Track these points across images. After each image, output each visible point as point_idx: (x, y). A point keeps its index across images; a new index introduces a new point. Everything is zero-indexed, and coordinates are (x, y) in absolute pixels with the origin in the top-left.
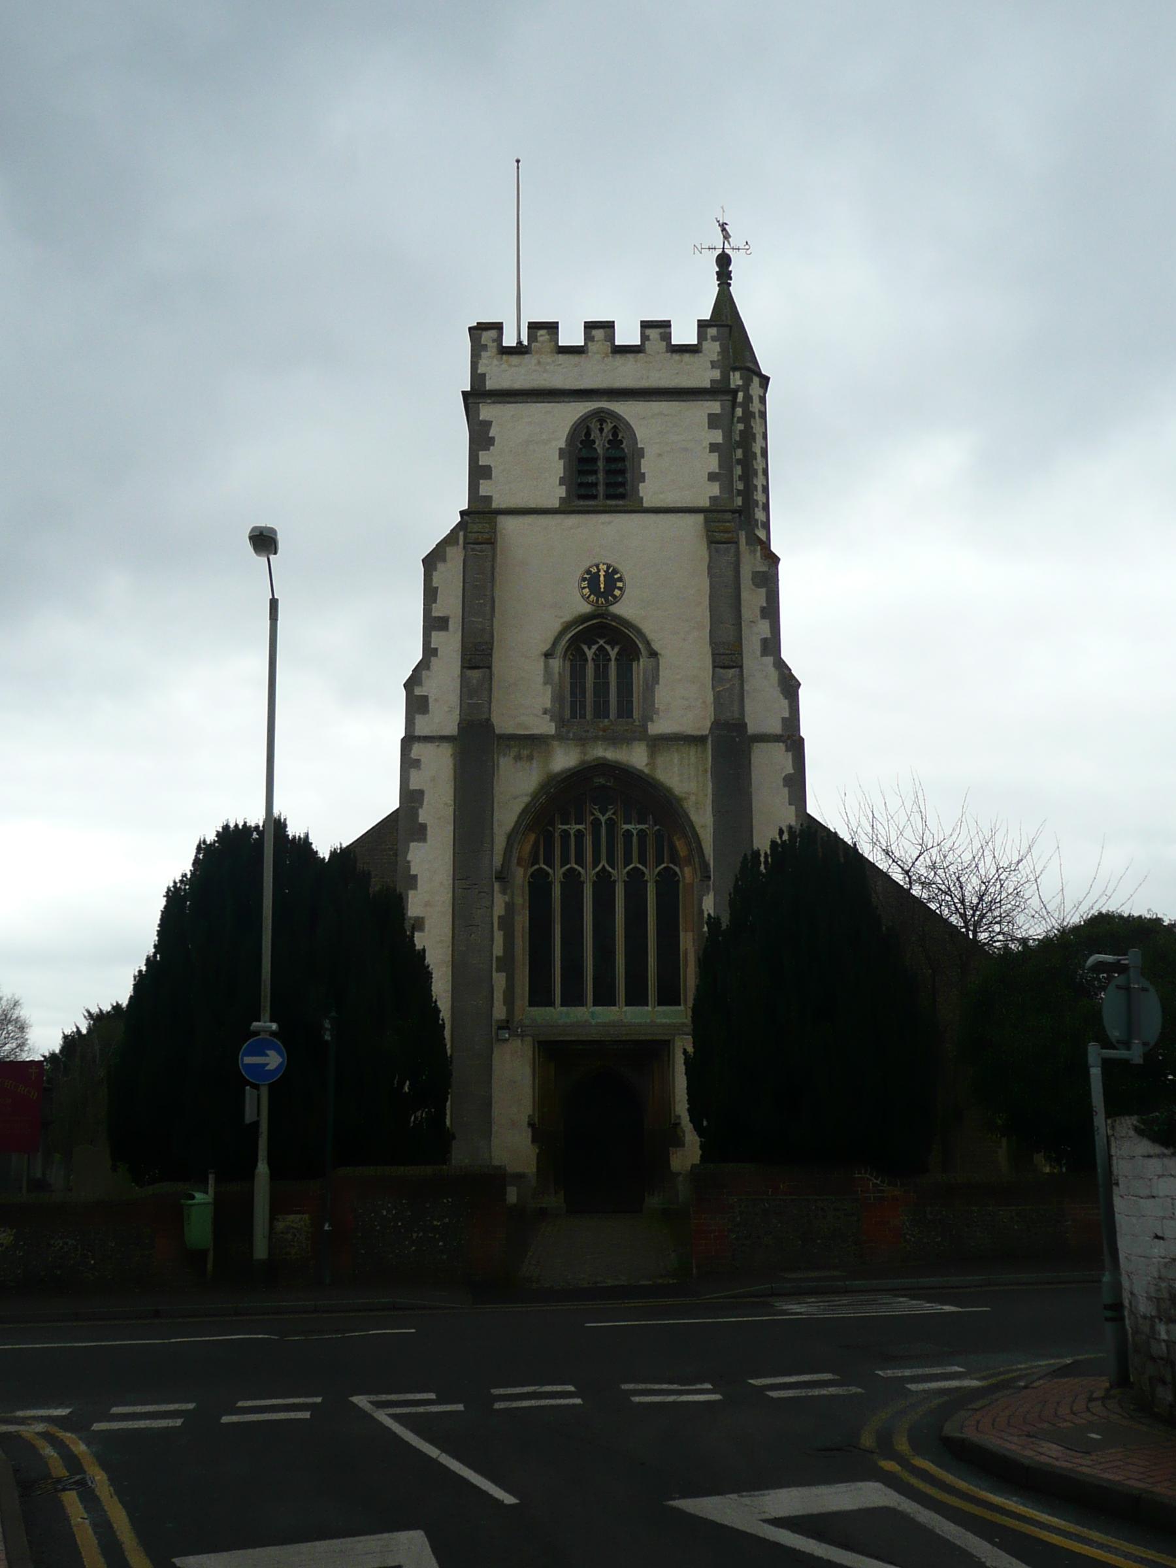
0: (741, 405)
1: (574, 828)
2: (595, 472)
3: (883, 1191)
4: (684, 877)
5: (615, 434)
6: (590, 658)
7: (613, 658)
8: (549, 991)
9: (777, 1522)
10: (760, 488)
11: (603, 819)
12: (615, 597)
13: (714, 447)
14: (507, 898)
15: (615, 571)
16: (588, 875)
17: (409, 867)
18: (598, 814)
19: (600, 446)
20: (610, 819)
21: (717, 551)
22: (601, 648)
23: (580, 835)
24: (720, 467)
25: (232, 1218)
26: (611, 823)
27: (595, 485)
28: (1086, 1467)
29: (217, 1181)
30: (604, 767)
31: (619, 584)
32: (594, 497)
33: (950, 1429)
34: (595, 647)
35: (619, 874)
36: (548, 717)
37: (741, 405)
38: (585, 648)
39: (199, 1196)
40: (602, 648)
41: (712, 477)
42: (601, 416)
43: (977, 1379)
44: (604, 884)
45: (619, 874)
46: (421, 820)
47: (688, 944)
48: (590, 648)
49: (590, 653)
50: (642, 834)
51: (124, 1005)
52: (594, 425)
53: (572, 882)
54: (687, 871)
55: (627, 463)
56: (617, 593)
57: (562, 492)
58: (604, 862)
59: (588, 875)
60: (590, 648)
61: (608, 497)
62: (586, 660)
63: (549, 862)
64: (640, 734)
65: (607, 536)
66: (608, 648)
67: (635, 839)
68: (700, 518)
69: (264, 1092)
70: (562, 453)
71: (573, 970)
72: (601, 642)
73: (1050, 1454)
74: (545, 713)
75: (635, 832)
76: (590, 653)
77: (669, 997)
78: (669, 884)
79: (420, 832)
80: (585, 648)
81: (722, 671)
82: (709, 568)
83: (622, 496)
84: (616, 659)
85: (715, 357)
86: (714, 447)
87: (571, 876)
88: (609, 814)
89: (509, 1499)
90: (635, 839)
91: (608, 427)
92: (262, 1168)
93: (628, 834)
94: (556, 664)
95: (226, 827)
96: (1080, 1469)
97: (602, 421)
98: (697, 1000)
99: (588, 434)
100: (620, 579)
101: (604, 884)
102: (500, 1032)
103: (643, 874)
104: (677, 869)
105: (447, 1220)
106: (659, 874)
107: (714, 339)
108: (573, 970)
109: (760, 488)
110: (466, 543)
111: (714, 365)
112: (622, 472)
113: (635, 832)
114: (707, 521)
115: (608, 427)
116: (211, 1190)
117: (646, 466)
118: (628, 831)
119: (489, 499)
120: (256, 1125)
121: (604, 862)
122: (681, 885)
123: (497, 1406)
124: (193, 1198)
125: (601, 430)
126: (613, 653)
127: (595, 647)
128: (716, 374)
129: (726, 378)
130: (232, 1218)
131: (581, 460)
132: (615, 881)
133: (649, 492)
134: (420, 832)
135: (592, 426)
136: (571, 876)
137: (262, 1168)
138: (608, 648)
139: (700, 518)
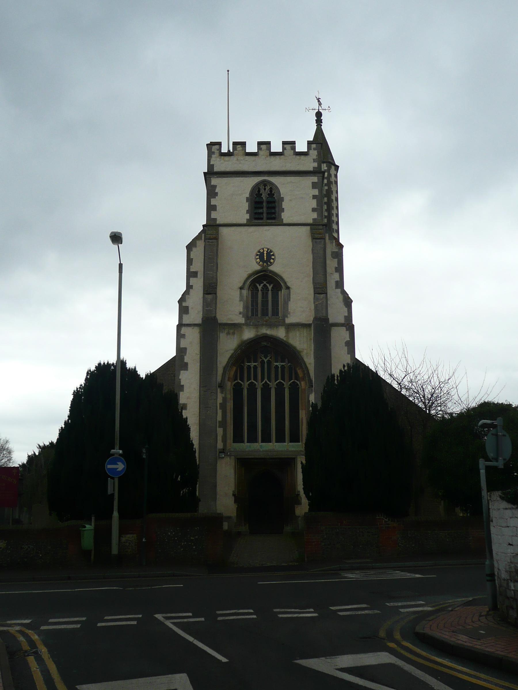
0: (326, 178)
1: (253, 364)
2: (262, 208)
3: (389, 524)
4: (301, 386)
5: (271, 191)
6: (260, 290)
7: (270, 290)
8: (242, 436)
9: (342, 670)
10: (335, 215)
11: (266, 360)
12: (271, 263)
14: (223, 395)
15: (271, 251)
16: (259, 385)
17: (180, 382)
18: (263, 358)
20: (269, 360)
21: (316, 242)
22: (265, 285)
23: (255, 367)
24: (317, 205)
25: (102, 536)
26: (269, 362)
27: (262, 213)
28: (478, 645)
29: (96, 520)
31: (273, 257)
32: (262, 219)
33: (419, 629)
34: (262, 285)
35: (273, 385)
36: (241, 316)
37: (326, 178)
38: (258, 285)
39: (88, 527)
41: (314, 210)
42: (265, 183)
43: (430, 607)
44: (266, 389)
45: (273, 385)
46: (185, 361)
47: (303, 415)
48: (260, 285)
49: (260, 288)
50: (283, 367)
51: (55, 442)
52: (262, 187)
53: (252, 388)
54: (303, 383)
55: (276, 204)
56: (272, 261)
57: (247, 216)
58: (266, 380)
59: (259, 385)
60: (260, 285)
61: (268, 219)
62: (258, 290)
63: (242, 379)
64: (282, 323)
65: (267, 236)
66: (268, 285)
67: (280, 369)
68: (308, 228)
69: (116, 481)
70: (247, 199)
71: (252, 427)
72: (265, 283)
73: (462, 640)
74: (240, 314)
75: (280, 366)
76: (260, 288)
77: (295, 439)
78: (295, 389)
80: (258, 285)
81: (318, 295)
82: (312, 250)
83: (274, 218)
84: (271, 290)
85: (315, 157)
87: (252, 385)
88: (268, 358)
90: (280, 369)
91: (268, 188)
92: (116, 514)
93: (277, 367)
94: (245, 292)
95: (100, 364)
96: (476, 646)
97: (265, 185)
98: (307, 440)
99: (259, 191)
100: (273, 255)
101: (266, 389)
102: (220, 454)
103: (283, 384)
104: (298, 383)
105: (197, 537)
106: (290, 385)
107: (314, 149)
108: (252, 427)
109: (335, 215)
110: (205, 239)
111: (314, 161)
112: (274, 208)
113: (280, 366)
114: (311, 229)
115: (268, 188)
116: (93, 524)
118: (277, 366)
119: (215, 219)
120: (113, 495)
121: (266, 380)
122: (300, 389)
123: (219, 619)
124: (85, 527)
125: (265, 189)
126: (270, 288)
127: (262, 285)
128: (316, 165)
129: (320, 166)
130: (102, 536)
132: (271, 388)
135: (261, 187)
136: (252, 385)
137: (116, 514)
138: (268, 285)
139: (308, 228)
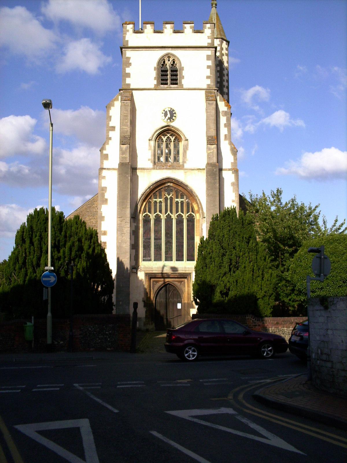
0: (219, 51)
1: (158, 200)
2: (167, 75)
3: (255, 323)
4: (196, 217)
5: (174, 62)
6: (164, 141)
7: (172, 141)
8: (150, 256)
9: (192, 417)
10: (225, 81)
11: (169, 197)
12: (173, 120)
13: (208, 67)
14: (135, 224)
15: (173, 110)
16: (163, 217)
17: (102, 213)
18: (167, 195)
19: (168, 64)
20: (171, 197)
21: (209, 103)
22: (168, 138)
23: (160, 202)
24: (211, 74)
25: (40, 330)
26: (171, 199)
27: (167, 80)
28: (290, 402)
29: (35, 318)
30: (169, 180)
31: (175, 115)
32: (167, 84)
33: (257, 393)
34: (166, 137)
35: (174, 216)
36: (150, 161)
37: (219, 51)
38: (163, 137)
39: (29, 324)
40: (168, 135)
41: (208, 77)
42: (168, 56)
43: (271, 380)
44: (169, 220)
45: (174, 216)
46: (106, 197)
47: (197, 241)
48: (164, 137)
49: (164, 139)
50: (182, 203)
51: (7, 260)
52: (166, 59)
53: (158, 220)
54: (198, 215)
55: (178, 72)
56: (174, 118)
57: (155, 82)
58: (169, 212)
59: (163, 217)
60: (164, 137)
61: (172, 84)
62: (163, 141)
63: (150, 212)
64: (181, 167)
65: (169, 97)
66: (171, 137)
67: (180, 204)
68: (204, 91)
69: (49, 289)
70: (155, 69)
71: (158, 248)
72: (169, 135)
73: (281, 399)
74: (149, 160)
75: (180, 202)
76: (164, 139)
77: (190, 258)
78: (191, 221)
79: (105, 201)
80: (163, 137)
81: (210, 146)
82: (206, 110)
83: (177, 84)
84: (174, 141)
85: (210, 35)
86: (208, 67)
87: (180, 216)
88: (171, 195)
89: (116, 411)
90: (180, 204)
91: (171, 59)
92: (49, 314)
93: (177, 203)
94: (152, 143)
95: (313, 153)
96: (300, 405)
97: (169, 57)
98: (198, 259)
99: (164, 62)
100: (175, 113)
101: (169, 220)
102: (133, 270)
103: (182, 216)
104: (194, 214)
105: (110, 332)
106: (188, 216)
107: (209, 28)
108: (158, 248)
109: (225, 81)
110: (121, 101)
111: (208, 37)
112: (177, 75)
113: (180, 202)
114: (206, 92)
115: (171, 59)
116: (33, 321)
117: (184, 73)
118: (177, 201)
119: (129, 85)
120: (47, 300)
121: (169, 212)
122: (195, 220)
123: (118, 387)
124: (26, 324)
125: (169, 60)
126: (173, 139)
127: (166, 137)
128: (210, 41)
129: (213, 42)
130: (40, 330)
131: (162, 71)
132: (172, 219)
133: (185, 82)
134: (105, 201)
135: (165, 59)
136: (180, 216)
137: (49, 314)
138: (171, 137)
139: (204, 91)
